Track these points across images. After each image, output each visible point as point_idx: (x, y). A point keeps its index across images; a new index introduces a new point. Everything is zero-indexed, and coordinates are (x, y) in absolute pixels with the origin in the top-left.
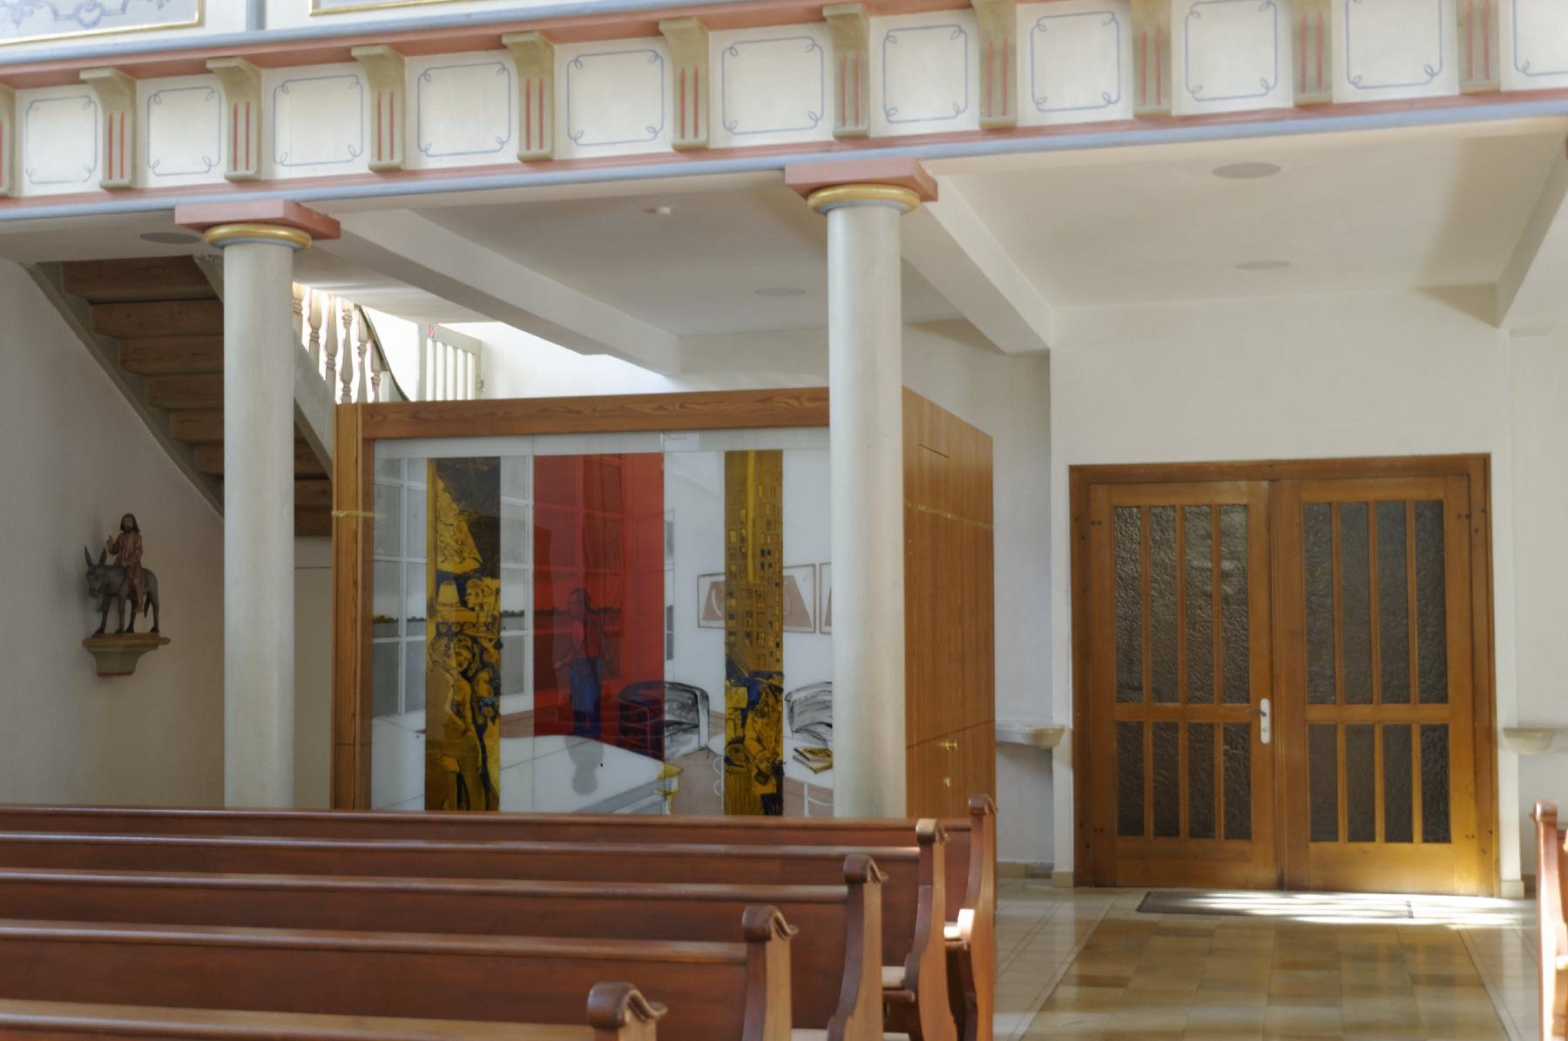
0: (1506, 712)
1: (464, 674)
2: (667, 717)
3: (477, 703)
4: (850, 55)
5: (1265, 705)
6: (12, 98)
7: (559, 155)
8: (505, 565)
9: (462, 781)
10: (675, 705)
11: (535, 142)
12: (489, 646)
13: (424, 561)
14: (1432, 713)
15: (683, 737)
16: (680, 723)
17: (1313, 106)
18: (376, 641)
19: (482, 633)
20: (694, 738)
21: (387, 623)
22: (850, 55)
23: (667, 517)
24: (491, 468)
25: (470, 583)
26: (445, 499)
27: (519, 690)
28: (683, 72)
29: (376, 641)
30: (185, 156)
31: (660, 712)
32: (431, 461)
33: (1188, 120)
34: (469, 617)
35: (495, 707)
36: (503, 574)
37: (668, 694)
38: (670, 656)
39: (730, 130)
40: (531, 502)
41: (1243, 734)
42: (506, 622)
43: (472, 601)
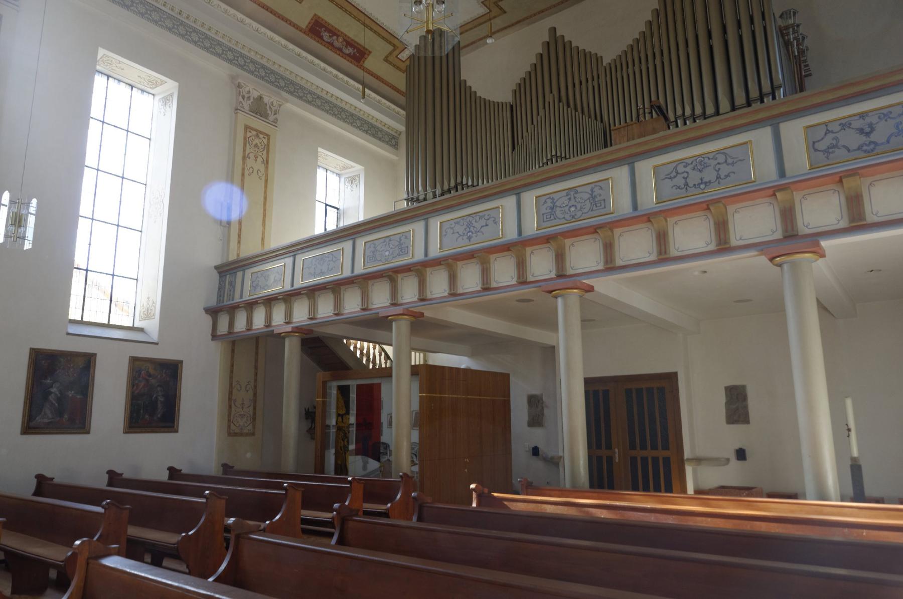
0: (687, 454)
5: (617, 450)
8: (351, 412)
9: (342, 468)
14: (666, 453)
17: (486, 289)
21: (328, 426)
24: (348, 387)
30: (325, 309)
41: (610, 459)
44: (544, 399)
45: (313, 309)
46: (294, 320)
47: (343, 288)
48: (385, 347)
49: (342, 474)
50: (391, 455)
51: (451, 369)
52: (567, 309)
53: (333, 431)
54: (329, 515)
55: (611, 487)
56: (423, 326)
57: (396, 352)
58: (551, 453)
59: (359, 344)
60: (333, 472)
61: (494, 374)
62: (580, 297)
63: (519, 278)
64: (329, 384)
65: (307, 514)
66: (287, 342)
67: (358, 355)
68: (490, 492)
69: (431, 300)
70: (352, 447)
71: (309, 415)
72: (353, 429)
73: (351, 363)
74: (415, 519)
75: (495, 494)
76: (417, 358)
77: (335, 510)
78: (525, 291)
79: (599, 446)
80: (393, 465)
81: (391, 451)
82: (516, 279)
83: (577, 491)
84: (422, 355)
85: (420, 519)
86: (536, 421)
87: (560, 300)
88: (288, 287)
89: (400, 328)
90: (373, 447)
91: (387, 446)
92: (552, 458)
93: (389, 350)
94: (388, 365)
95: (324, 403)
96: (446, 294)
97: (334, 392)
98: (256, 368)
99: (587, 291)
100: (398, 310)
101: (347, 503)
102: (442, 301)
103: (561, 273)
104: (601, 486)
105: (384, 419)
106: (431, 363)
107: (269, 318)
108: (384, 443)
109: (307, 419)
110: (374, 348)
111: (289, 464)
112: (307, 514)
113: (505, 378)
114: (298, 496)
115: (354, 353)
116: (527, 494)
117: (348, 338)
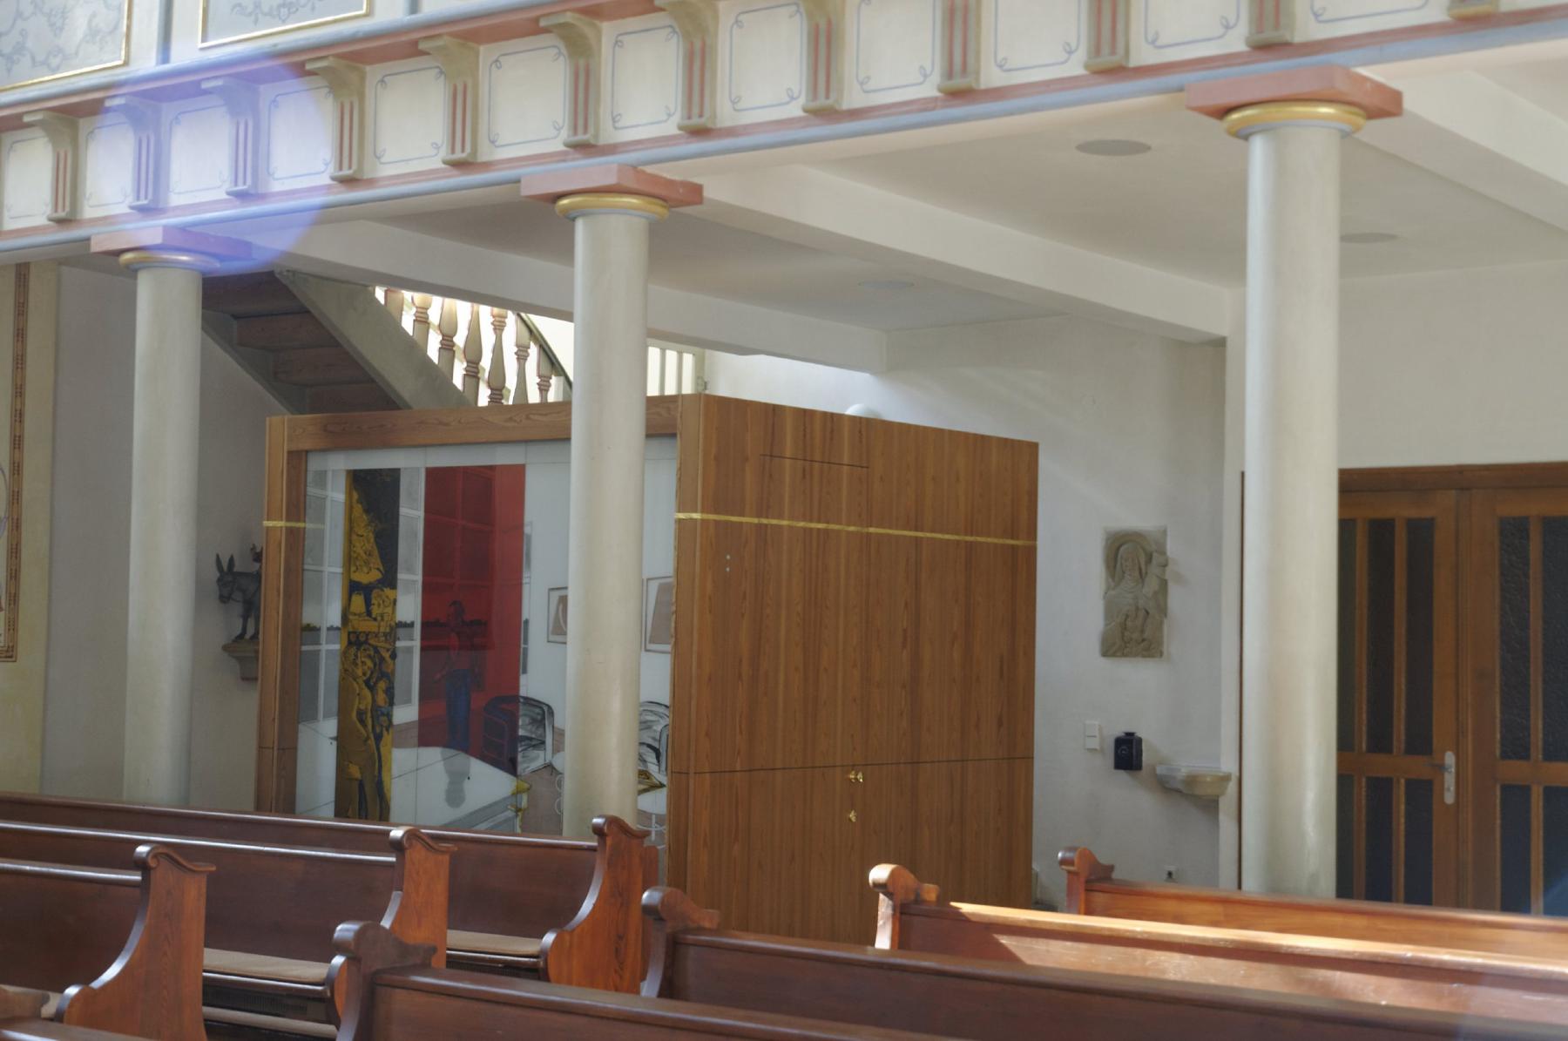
1: (367, 683)
2: (521, 732)
3: (375, 708)
4: (582, 62)
5: (1450, 759)
6: (74, 127)
7: (483, 157)
8: (401, 576)
9: (363, 794)
10: (527, 720)
11: (1106, 49)
12: (387, 655)
13: (340, 570)
15: (533, 753)
16: (531, 739)
17: (961, 93)
18: (304, 648)
19: (381, 643)
20: (541, 753)
21: (312, 630)
22: (582, 62)
23: (527, 530)
25: (375, 593)
26: (358, 509)
27: (408, 701)
28: (692, 44)
29: (304, 648)
31: (515, 727)
32: (349, 472)
33: (855, 114)
34: (370, 626)
35: (389, 716)
36: (399, 584)
37: (522, 710)
38: (525, 672)
39: (493, 142)
40: (421, 513)
41: (1422, 792)
42: (401, 632)
43: (375, 611)
44: (1172, 548)
45: (251, 156)
46: (175, 200)
47: (373, 72)
48: (542, 323)
49: (364, 817)
50: (558, 748)
51: (805, 415)
52: (1287, 184)
53: (330, 649)
54: (303, 972)
55: (1420, 894)
56: (686, 231)
57: (590, 346)
58: (1185, 765)
59: (437, 306)
60: (330, 810)
61: (979, 443)
62: (1345, 135)
63: (1096, 50)
64: (314, 464)
65: (226, 963)
66: (145, 287)
67: (433, 351)
68: (944, 899)
69: (731, 132)
70: (406, 713)
71: (239, 588)
72: (411, 645)
73: (404, 384)
74: (650, 988)
75: (966, 908)
76: (669, 372)
77: (340, 948)
78: (1122, 105)
79: (1380, 742)
80: (568, 785)
81: (559, 735)
82: (1081, 55)
83: (1283, 907)
84: (688, 359)
85: (669, 990)
86: (1134, 633)
87: (1258, 148)
88: (146, 63)
89: (608, 245)
90: (485, 709)
91: (542, 713)
92: (1192, 780)
93: (560, 336)
94: (553, 396)
95: (295, 539)
96: (795, 110)
97: (336, 496)
98: (19, 391)
99: (1373, 114)
100: (598, 171)
101: (386, 923)
102: (777, 138)
103: (1270, 35)
104: (1379, 891)
105: (535, 607)
106: (723, 389)
107: (68, 183)
108: (531, 702)
109: (224, 599)
110: (499, 327)
111: (154, 776)
112: (226, 963)
113: (1023, 456)
114: (194, 894)
115: (441, 376)
116: (1089, 911)
117: (395, 283)
